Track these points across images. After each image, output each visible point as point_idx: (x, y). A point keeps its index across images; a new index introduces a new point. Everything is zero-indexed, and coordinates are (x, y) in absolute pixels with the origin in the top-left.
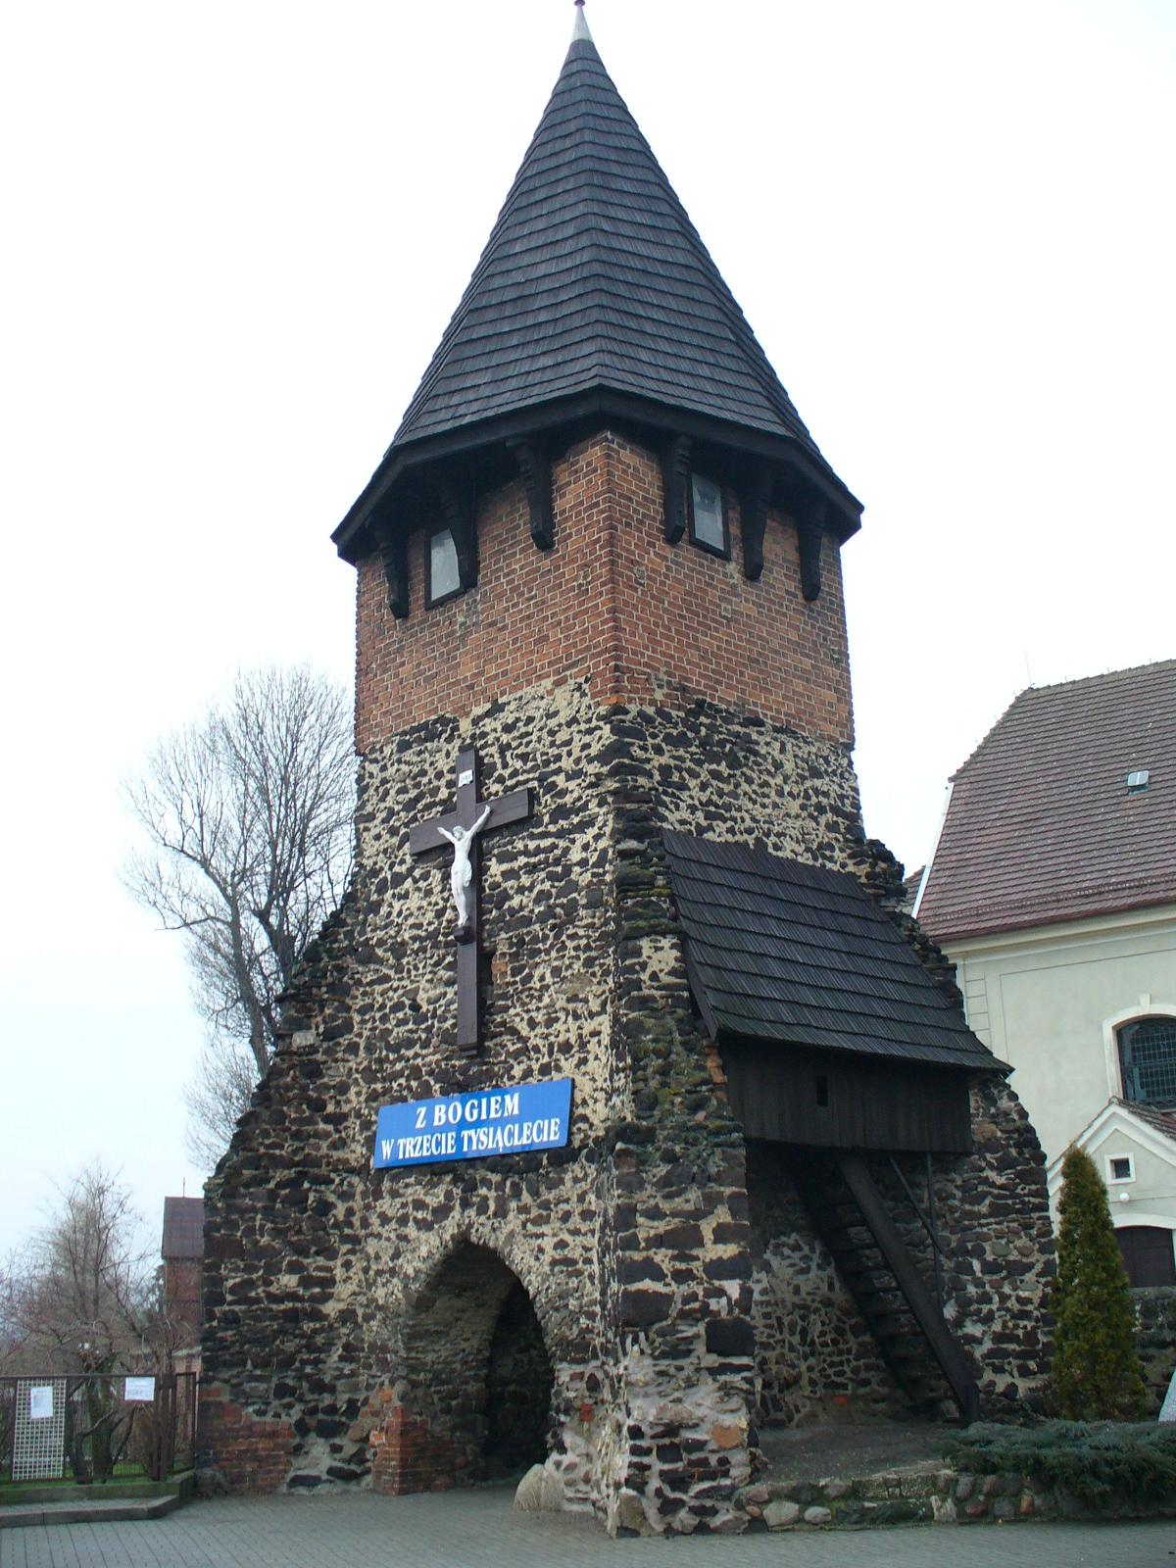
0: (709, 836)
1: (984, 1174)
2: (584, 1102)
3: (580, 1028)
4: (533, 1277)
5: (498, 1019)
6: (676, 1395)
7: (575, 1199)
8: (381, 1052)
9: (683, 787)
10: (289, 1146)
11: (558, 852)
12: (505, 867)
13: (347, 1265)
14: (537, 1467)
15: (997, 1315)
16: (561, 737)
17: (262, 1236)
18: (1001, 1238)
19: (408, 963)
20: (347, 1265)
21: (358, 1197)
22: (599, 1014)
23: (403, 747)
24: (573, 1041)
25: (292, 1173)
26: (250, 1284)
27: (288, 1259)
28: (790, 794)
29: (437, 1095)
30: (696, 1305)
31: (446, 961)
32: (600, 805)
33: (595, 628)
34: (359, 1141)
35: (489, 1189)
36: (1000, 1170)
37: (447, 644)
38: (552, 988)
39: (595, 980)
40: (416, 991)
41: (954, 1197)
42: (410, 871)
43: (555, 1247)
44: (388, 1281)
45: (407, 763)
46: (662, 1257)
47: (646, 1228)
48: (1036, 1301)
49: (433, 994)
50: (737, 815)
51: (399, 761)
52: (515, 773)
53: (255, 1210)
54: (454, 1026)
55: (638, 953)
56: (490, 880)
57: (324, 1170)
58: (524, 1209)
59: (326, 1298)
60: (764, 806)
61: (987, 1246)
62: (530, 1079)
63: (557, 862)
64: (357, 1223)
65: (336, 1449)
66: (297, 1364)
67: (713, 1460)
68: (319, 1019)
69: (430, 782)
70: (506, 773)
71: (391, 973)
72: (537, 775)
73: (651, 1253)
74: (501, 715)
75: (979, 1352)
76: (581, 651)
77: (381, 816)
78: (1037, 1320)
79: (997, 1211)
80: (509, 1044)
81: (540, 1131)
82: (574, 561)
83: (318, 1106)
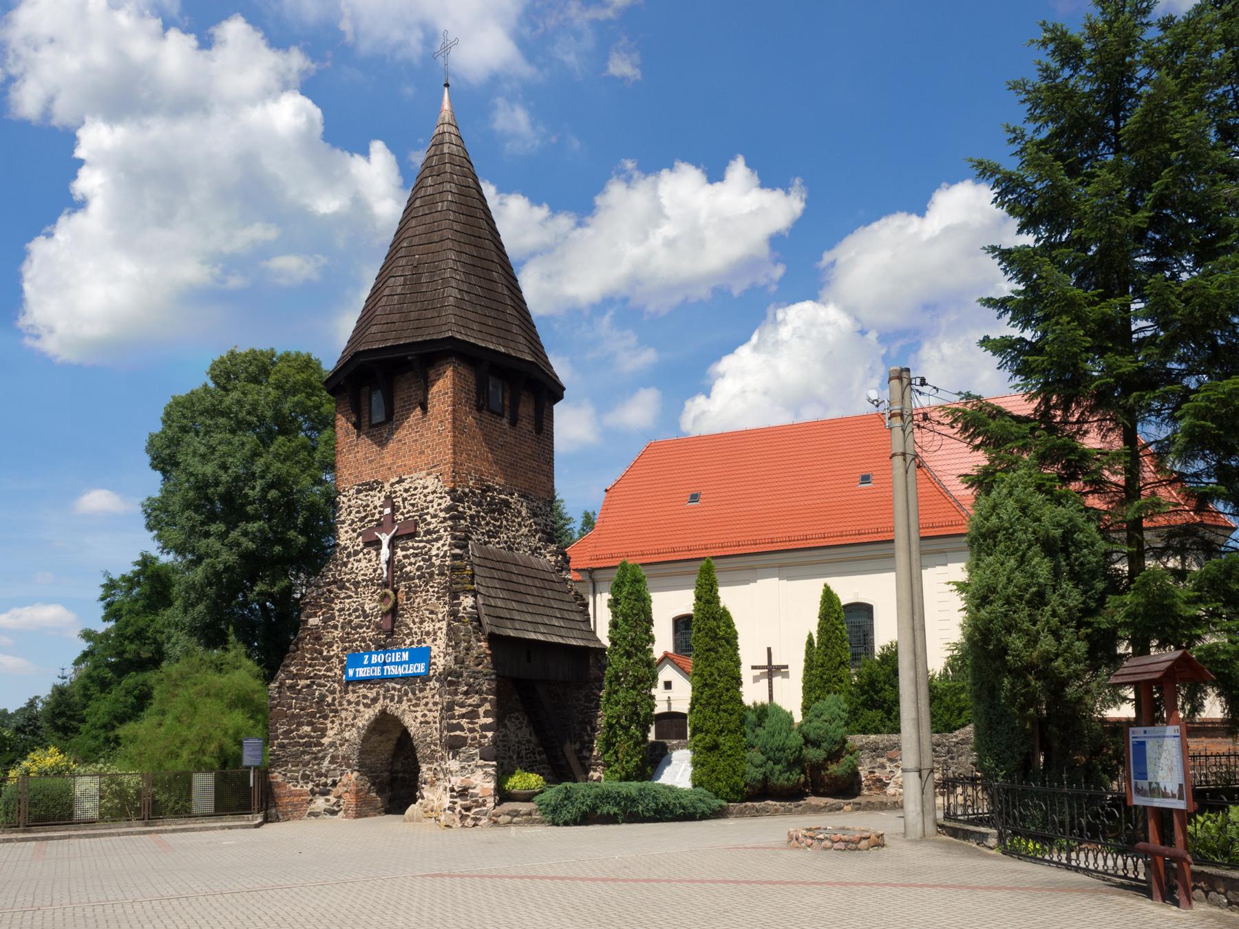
9: (479, 525)
12: (404, 553)
13: (333, 722)
16: (430, 498)
20: (333, 722)
23: (359, 492)
25: (308, 682)
40: (364, 604)
45: (361, 500)
46: (464, 722)
47: (458, 711)
57: (322, 681)
59: (323, 735)
63: (426, 553)
65: (328, 800)
67: (480, 800)
70: (405, 511)
83: (321, 653)
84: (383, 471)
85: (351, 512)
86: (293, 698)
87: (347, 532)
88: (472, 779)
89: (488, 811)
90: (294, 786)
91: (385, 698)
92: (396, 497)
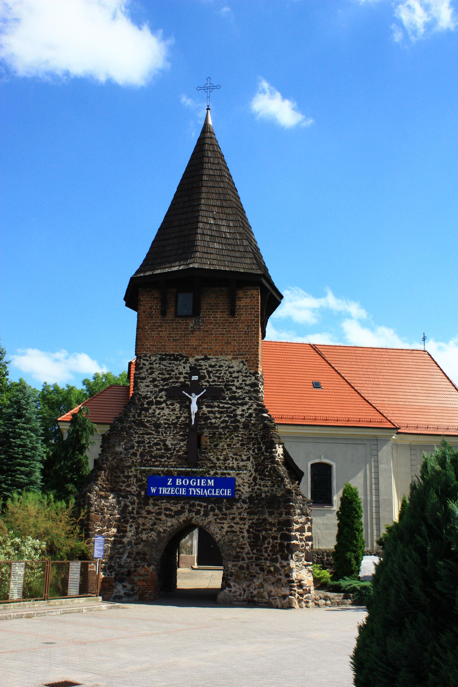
7: (237, 514)
8: (147, 457)
12: (209, 409)
13: (131, 526)
16: (235, 375)
19: (162, 431)
20: (131, 526)
21: (136, 504)
22: (246, 461)
23: (161, 359)
39: (245, 451)
40: (166, 440)
43: (228, 527)
45: (164, 365)
46: (298, 534)
59: (124, 536)
63: (231, 412)
65: (124, 587)
66: (115, 558)
69: (176, 374)
70: (211, 380)
71: (154, 432)
74: (209, 361)
76: (245, 351)
77: (149, 380)
87: (148, 386)
91: (190, 511)
92: (202, 369)
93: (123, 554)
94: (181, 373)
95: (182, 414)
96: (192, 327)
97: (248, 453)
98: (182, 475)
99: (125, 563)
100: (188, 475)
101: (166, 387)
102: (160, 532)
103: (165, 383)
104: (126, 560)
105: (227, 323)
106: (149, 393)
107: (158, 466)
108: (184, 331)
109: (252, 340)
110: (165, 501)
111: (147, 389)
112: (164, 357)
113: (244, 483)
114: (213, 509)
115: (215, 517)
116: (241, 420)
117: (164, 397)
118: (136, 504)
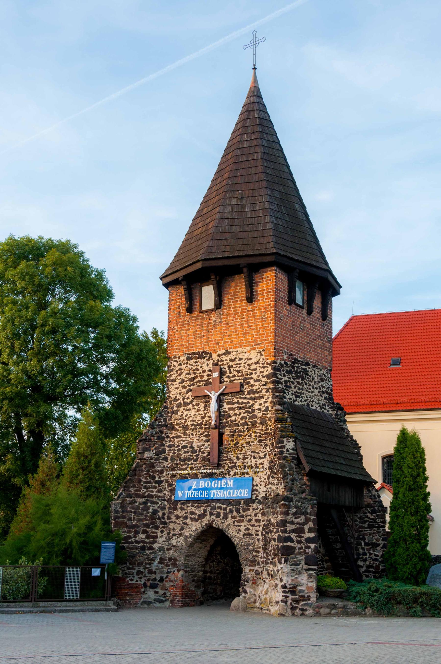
0: (296, 403)
1: (367, 515)
2: (257, 485)
3: (256, 461)
4: (236, 539)
5: (225, 455)
6: (296, 576)
7: (253, 515)
8: (177, 461)
9: (290, 387)
10: (143, 491)
11: (250, 404)
12: (230, 406)
13: (162, 532)
14: (236, 599)
15: (368, 559)
17: (134, 521)
18: (371, 535)
19: (189, 433)
20: (162, 532)
21: (167, 509)
22: (263, 458)
23: (189, 359)
24: (253, 465)
25: (143, 500)
26: (130, 537)
27: (142, 529)
28: (316, 388)
29: (200, 477)
30: (302, 550)
31: (205, 434)
32: (266, 392)
33: (267, 334)
34: (167, 490)
35: (221, 510)
36: (372, 513)
37: (208, 326)
38: (246, 448)
39: (262, 447)
40: (192, 442)
41: (357, 521)
42: (191, 402)
43: (245, 530)
44: (178, 538)
45: (191, 365)
46: (293, 535)
47: (289, 527)
48: (380, 556)
49: (199, 444)
50: (302, 395)
51: (187, 363)
52: (234, 376)
53: (131, 512)
54: (207, 455)
55: (283, 442)
56: (223, 410)
57: (154, 499)
58: (233, 517)
59: (154, 542)
60: (309, 392)
61: (366, 537)
62: (236, 476)
63: (249, 408)
64: (166, 518)
65: (156, 592)
66: (144, 564)
67: (306, 596)
68: (154, 448)
69: (200, 373)
70: (231, 375)
71: (182, 435)
72: (243, 378)
73: (290, 534)
74: (229, 355)
75: (362, 570)
76: (262, 340)
77: (178, 381)
78: (380, 562)
79: (370, 527)
80: (229, 464)
81: (241, 493)
82: (260, 309)
83: (154, 477)
84: (211, 345)
85: (181, 374)
86: (131, 512)
87: (177, 388)
88: (299, 579)
89: (311, 604)
90: (131, 580)
91: (211, 514)
92: (223, 365)
93: (154, 560)
94: (204, 371)
95: (206, 414)
96: (214, 321)
97: (264, 450)
98: (205, 476)
99: (157, 569)
100: (211, 476)
101: (191, 388)
102: (187, 537)
103: (192, 383)
104: (157, 566)
105: (245, 312)
106: (178, 395)
107: (185, 469)
108: (208, 326)
109: (268, 327)
110: (190, 505)
111: (177, 390)
112: (191, 356)
113: (261, 482)
114: (231, 511)
115: (233, 520)
116: (258, 414)
117: (190, 397)
118: (167, 509)
